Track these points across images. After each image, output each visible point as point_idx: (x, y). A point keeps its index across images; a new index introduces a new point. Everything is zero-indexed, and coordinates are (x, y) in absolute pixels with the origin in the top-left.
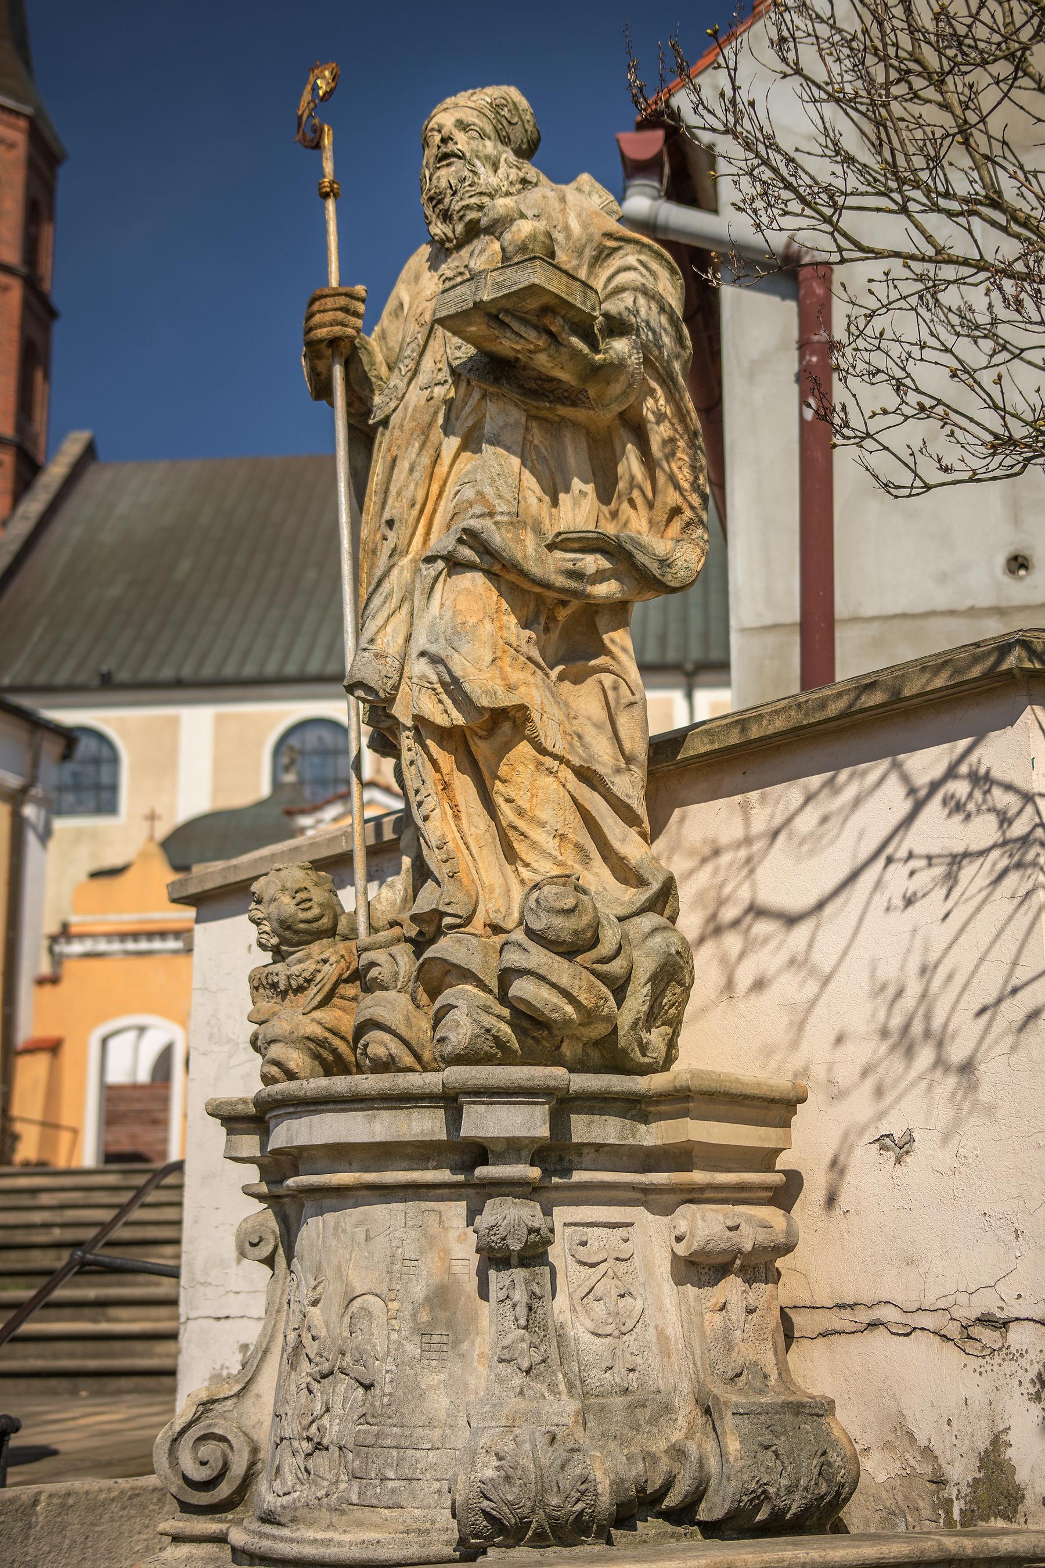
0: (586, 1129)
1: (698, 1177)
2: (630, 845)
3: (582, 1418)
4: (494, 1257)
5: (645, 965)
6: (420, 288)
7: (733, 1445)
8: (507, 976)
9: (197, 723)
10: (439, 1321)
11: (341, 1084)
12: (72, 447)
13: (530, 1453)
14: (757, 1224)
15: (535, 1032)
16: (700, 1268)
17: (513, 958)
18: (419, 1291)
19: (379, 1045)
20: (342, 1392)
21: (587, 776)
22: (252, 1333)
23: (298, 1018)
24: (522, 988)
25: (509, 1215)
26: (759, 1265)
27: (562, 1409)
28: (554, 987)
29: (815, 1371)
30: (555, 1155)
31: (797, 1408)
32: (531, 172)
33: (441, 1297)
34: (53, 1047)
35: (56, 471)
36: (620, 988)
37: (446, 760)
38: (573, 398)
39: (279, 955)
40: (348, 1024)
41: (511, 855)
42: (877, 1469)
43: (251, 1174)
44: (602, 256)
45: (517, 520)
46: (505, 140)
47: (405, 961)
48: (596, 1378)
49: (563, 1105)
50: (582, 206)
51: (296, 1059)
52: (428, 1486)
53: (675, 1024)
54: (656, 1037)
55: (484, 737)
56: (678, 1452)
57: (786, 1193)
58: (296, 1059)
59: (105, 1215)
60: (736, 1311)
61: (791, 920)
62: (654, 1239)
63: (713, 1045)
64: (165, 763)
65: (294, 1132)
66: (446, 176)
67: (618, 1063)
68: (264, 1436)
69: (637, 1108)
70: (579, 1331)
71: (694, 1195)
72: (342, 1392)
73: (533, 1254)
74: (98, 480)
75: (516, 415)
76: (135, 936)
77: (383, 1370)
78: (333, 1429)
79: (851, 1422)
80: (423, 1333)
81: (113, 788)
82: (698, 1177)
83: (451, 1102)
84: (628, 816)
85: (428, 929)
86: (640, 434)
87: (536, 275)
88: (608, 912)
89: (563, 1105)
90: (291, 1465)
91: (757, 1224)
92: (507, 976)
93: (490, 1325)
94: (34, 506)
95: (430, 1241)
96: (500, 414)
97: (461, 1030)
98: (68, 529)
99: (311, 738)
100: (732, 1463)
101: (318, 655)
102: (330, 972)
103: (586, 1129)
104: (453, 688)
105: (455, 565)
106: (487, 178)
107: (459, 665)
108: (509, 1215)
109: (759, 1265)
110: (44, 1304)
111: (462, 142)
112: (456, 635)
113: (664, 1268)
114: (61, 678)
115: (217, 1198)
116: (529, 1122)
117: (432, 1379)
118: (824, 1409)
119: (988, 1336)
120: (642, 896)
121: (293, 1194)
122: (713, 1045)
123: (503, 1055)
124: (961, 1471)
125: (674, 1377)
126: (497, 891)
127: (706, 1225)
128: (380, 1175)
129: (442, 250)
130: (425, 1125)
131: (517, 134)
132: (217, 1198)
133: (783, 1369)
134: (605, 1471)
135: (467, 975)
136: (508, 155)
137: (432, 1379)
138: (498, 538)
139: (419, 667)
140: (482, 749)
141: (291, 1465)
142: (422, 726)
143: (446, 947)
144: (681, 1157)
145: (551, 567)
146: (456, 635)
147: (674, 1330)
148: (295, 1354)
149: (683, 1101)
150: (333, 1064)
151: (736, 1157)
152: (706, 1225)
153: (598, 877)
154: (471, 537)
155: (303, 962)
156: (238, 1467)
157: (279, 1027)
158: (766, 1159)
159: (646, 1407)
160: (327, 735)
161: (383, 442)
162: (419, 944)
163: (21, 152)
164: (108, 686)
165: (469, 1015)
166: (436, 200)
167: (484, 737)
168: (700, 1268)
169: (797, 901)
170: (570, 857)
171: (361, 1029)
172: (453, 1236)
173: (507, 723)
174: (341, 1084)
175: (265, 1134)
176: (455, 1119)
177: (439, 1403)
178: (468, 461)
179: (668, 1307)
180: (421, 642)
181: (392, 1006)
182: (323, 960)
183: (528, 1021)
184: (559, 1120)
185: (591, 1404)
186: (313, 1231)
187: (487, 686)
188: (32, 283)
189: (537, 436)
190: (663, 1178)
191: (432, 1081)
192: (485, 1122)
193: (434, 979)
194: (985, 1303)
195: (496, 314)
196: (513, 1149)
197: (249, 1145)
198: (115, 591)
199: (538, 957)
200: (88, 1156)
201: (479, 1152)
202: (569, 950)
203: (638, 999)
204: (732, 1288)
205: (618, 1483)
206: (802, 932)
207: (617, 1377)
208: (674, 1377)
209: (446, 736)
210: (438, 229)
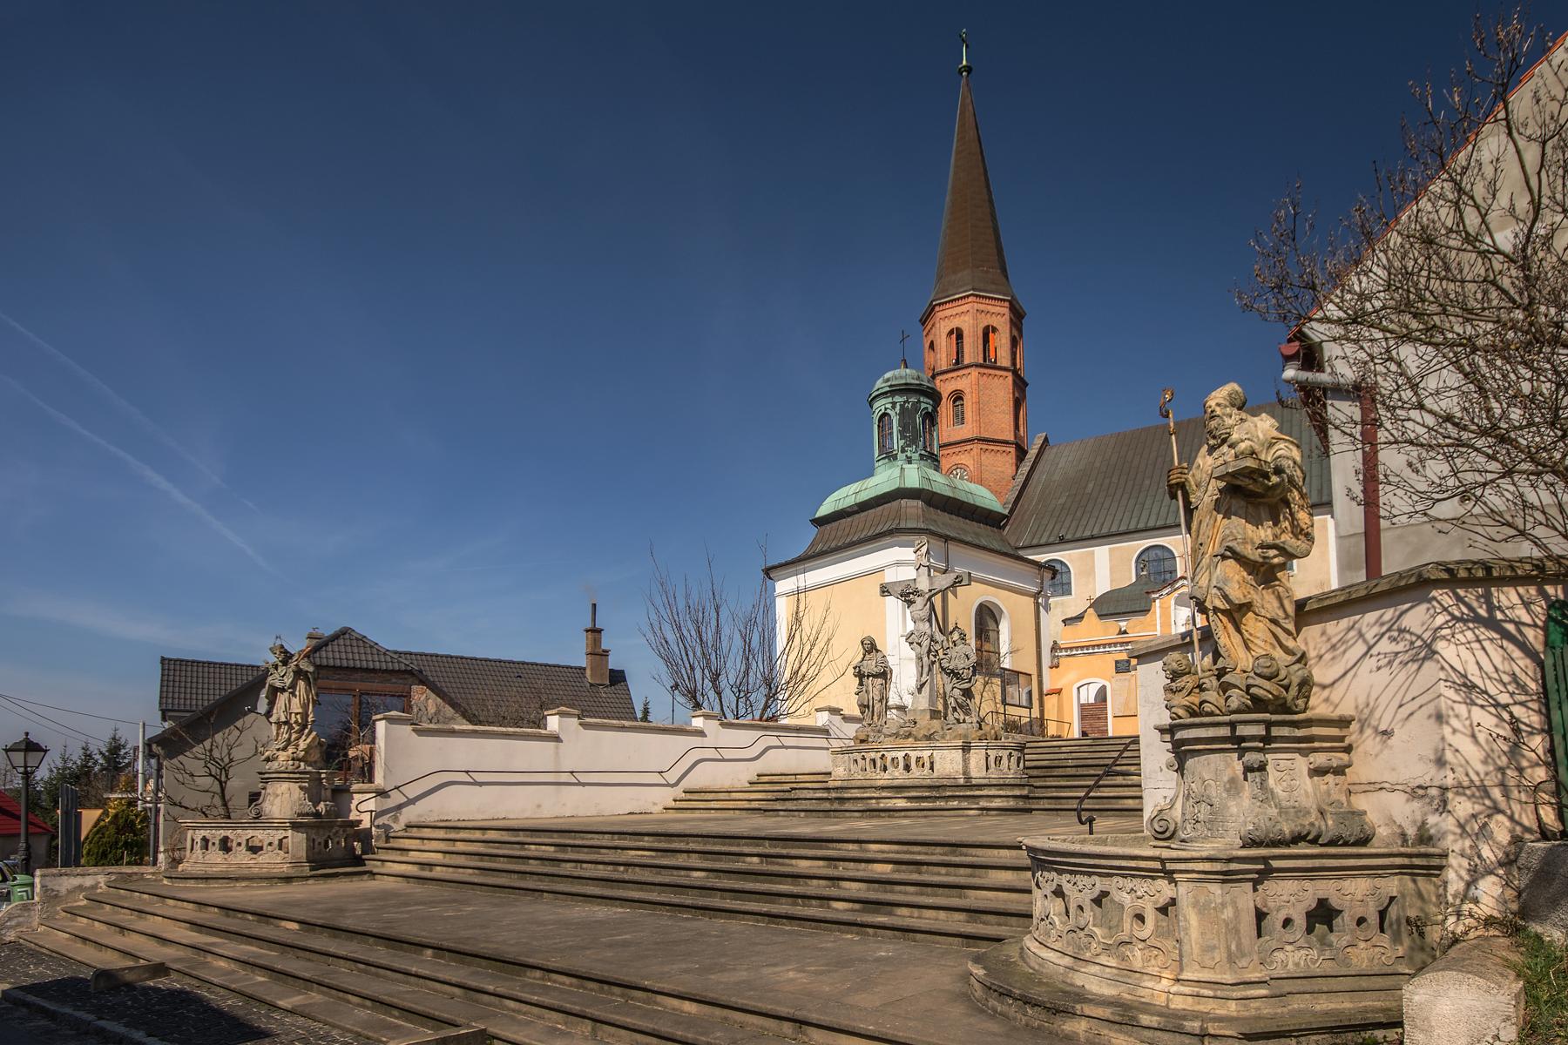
0: (1275, 731)
1: (1316, 744)
2: (1290, 643)
3: (1280, 813)
4: (1248, 769)
5: (1296, 681)
6: (1206, 462)
7: (1330, 822)
8: (1249, 687)
9: (1102, 554)
10: (1233, 787)
11: (1197, 720)
12: (1039, 442)
13: (1264, 824)
14: (1338, 759)
15: (1258, 704)
16: (1318, 772)
17: (1251, 681)
18: (1226, 779)
19: (1208, 707)
20: (1204, 807)
21: (1274, 621)
22: (1171, 794)
23: (1179, 700)
24: (1252, 690)
25: (1253, 758)
26: (1339, 771)
27: (1273, 812)
28: (1265, 689)
29: (1361, 802)
30: (1267, 739)
31: (1353, 813)
32: (1244, 415)
33: (1232, 781)
34: (1059, 692)
35: (1032, 453)
36: (1287, 688)
37: (1224, 619)
38: (1262, 496)
39: (1173, 680)
40: (1197, 701)
41: (1248, 648)
42: (1383, 832)
43: (1169, 746)
44: (1271, 445)
45: (1245, 542)
46: (1233, 405)
47: (1215, 683)
48: (1284, 804)
49: (1269, 725)
50: (1264, 425)
51: (1181, 712)
52: (1232, 832)
53: (1308, 697)
54: (1300, 702)
55: (1236, 613)
56: (1312, 824)
57: (1348, 749)
58: (1181, 712)
59: (1115, 755)
60: (1332, 784)
61: (1324, 687)
62: (1301, 764)
63: (1319, 706)
64: (1090, 572)
65: (1178, 735)
66: (1213, 424)
67: (1289, 711)
68: (1179, 819)
69: (1296, 724)
70: (1278, 790)
71: (1315, 750)
72: (1204, 807)
73: (1262, 768)
74: (1049, 455)
75: (1243, 503)
76: (1087, 647)
77: (1216, 801)
78: (1201, 817)
79: (1373, 817)
80: (1228, 791)
81: (1069, 583)
82: (1316, 744)
83: (1233, 725)
84: (1288, 632)
85: (1221, 673)
86: (1287, 504)
87: (1250, 463)
88: (1282, 664)
89: (1269, 725)
90: (1189, 827)
91: (1338, 759)
92: (1249, 687)
93: (1248, 789)
94: (1025, 468)
95: (1228, 765)
96: (1236, 503)
97: (1234, 703)
98: (1040, 477)
99: (1152, 554)
100: (1330, 826)
101: (1153, 517)
102: (1190, 685)
103: (1275, 731)
104: (1226, 597)
105: (1224, 557)
106: (1229, 422)
107: (1228, 590)
108: (1253, 758)
109: (1339, 771)
110: (1097, 786)
111: (1218, 411)
112: (1226, 580)
113: (1305, 772)
114: (1043, 541)
115: (1155, 756)
116: (1259, 730)
117: (1231, 803)
118: (1365, 813)
119: (1421, 792)
120: (1294, 659)
121: (1182, 754)
122: (1319, 706)
123: (1248, 710)
124: (1411, 832)
125: (1310, 804)
126: (1244, 660)
127: (1320, 759)
128: (1211, 746)
129: (1212, 450)
130: (1224, 732)
131: (1238, 402)
132: (1155, 756)
133: (1349, 802)
134: (1287, 829)
135: (1236, 687)
136: (1235, 411)
137: (1231, 803)
138: (1238, 549)
139: (1215, 591)
140: (1236, 615)
141: (1189, 827)
142: (1216, 610)
143: (1226, 678)
144: (1310, 739)
145: (1254, 555)
146: (1226, 580)
147: (1310, 790)
148: (1187, 797)
149: (1309, 723)
150: (1193, 714)
151: (1332, 741)
152: (1320, 759)
153: (1278, 653)
154: (1229, 549)
155: (1180, 683)
156: (1172, 828)
157: (1175, 702)
158: (1342, 739)
159: (1301, 812)
160: (1159, 552)
161: (1196, 514)
162: (1219, 677)
163: (1007, 317)
164: (1063, 541)
165: (1236, 698)
166: (1210, 432)
167: (1236, 613)
168: (1318, 772)
169: (1327, 681)
170: (1268, 647)
171: (1202, 703)
172: (1233, 764)
173: (1246, 607)
174: (1197, 720)
175: (1173, 735)
176: (1234, 729)
177: (1234, 810)
178: (1226, 521)
179: (1307, 784)
180: (1214, 583)
181: (1211, 696)
182: (1187, 682)
183: (1255, 699)
184: (1268, 730)
185: (1283, 811)
186: (1190, 763)
187: (1237, 595)
188: (1015, 373)
189: (1251, 509)
190: (1305, 745)
191: (1227, 718)
192: (1243, 731)
193: (1225, 688)
194: (1420, 782)
195: (1233, 475)
196: (1253, 738)
197: (1167, 738)
198: (1061, 501)
199: (1259, 681)
200: (1076, 734)
201: (1243, 739)
202: (1269, 679)
203: (1293, 691)
204: (1330, 778)
205: (1292, 832)
206: (1327, 692)
207: (1292, 803)
208: (1310, 804)
209: (1224, 612)
210: (1212, 442)
